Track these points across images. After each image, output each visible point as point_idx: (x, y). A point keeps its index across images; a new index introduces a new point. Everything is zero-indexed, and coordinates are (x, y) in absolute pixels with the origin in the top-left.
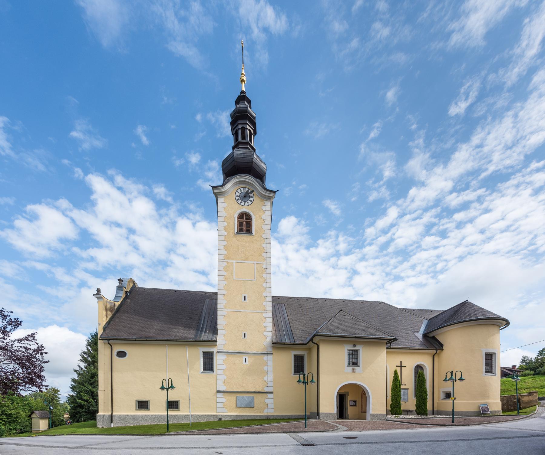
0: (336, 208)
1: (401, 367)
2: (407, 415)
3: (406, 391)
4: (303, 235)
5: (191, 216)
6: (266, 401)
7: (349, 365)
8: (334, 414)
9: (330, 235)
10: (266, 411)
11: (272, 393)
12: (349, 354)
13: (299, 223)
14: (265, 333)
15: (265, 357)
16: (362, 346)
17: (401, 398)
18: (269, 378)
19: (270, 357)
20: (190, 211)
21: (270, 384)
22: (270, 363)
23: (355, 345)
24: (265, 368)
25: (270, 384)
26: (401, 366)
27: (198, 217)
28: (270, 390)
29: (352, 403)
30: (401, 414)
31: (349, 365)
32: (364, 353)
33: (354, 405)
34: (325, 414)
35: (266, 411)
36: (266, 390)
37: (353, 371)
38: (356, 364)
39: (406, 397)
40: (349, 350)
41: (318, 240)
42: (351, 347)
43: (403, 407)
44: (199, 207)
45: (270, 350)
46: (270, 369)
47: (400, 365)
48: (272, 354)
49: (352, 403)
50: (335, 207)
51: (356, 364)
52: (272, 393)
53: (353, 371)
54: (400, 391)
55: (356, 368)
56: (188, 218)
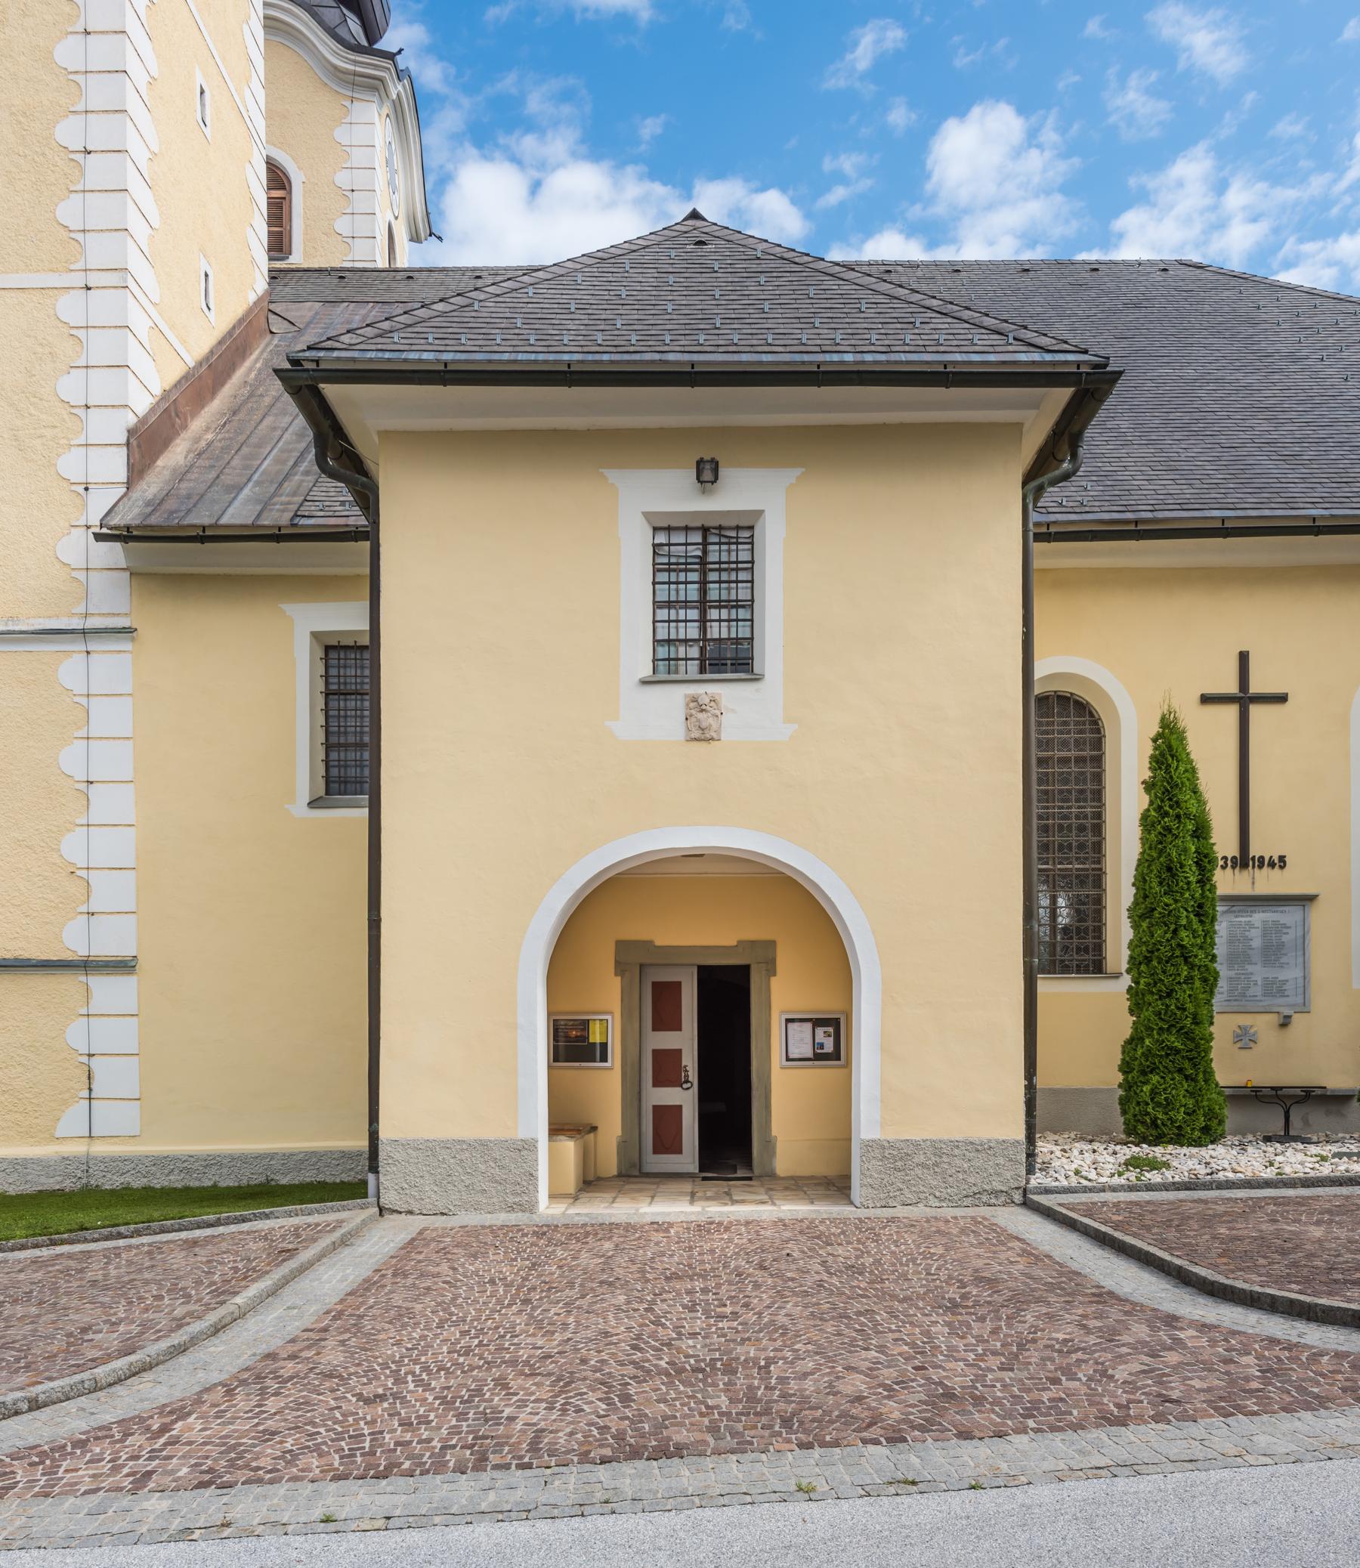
0: (1216, 44)
1: (1244, 699)
2: (1286, 1137)
3: (1290, 916)
4: (1048, 192)
5: (529, 143)
6: (76, 1035)
7: (665, 669)
8: (360, 1154)
9: (1180, 184)
10: (73, 1120)
11: (123, 966)
12: (664, 565)
13: (1032, 138)
14: (71, 465)
15: (71, 668)
16: (789, 476)
17: (1210, 981)
18: (107, 841)
19: (111, 665)
20: (531, 126)
21: (113, 892)
22: (112, 717)
23: (707, 473)
24: (72, 760)
25: (113, 892)
26: (1244, 699)
27: (558, 145)
28: (109, 944)
29: (802, 1041)
30: (1209, 1134)
31: (665, 669)
32: (808, 541)
33: (818, 1057)
34: (429, 1149)
35: (73, 1120)
36: (75, 943)
37: (701, 731)
38: (732, 659)
39: (1290, 974)
40: (663, 526)
41: (1117, 213)
42: (672, 492)
43: (1229, 1068)
44: (566, 96)
45: (110, 599)
46: (114, 761)
47: (1232, 687)
48: (128, 631)
49: (802, 1041)
50: (1216, 36)
51: (732, 659)
52: (123, 966)
53: (701, 731)
54: (1203, 913)
55: (729, 695)
56: (516, 160)
